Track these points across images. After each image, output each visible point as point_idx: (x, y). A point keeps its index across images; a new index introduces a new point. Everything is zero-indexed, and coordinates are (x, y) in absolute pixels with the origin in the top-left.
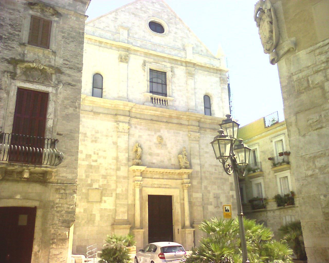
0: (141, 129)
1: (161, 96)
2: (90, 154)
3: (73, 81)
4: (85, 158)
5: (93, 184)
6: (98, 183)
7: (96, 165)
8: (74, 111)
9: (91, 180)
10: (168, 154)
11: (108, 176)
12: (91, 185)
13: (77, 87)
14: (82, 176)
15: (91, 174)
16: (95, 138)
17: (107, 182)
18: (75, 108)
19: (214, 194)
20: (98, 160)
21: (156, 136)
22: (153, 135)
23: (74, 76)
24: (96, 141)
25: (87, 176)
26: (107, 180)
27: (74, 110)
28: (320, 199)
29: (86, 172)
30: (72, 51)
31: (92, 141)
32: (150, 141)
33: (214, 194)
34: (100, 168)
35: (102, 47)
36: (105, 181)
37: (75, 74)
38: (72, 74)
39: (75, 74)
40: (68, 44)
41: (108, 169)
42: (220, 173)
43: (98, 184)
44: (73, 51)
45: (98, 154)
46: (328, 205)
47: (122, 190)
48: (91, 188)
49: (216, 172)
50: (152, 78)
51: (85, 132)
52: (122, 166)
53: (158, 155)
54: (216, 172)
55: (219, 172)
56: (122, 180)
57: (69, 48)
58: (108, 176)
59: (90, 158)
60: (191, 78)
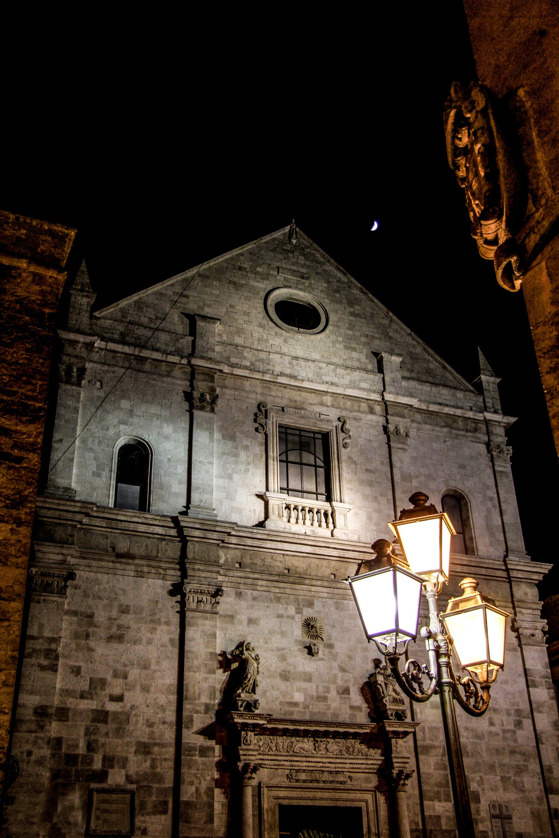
0: (254, 599)
1: (314, 502)
2: (101, 676)
3: (15, 446)
4: (87, 688)
5: (110, 770)
6: (124, 767)
7: (120, 710)
8: (12, 534)
9: (105, 759)
10: (340, 674)
11: (155, 744)
12: (102, 776)
13: (25, 465)
14: (77, 746)
15: (102, 740)
16: (119, 627)
17: (153, 767)
18: (14, 526)
19: (493, 806)
20: (126, 694)
21: (299, 620)
22: (293, 618)
23: (16, 432)
24: (120, 638)
25: (91, 747)
26: (153, 760)
27: (12, 530)
28: (35, 227)
29: (88, 732)
30: (16, 363)
31: (110, 639)
32: (283, 634)
33: (493, 806)
34: (133, 719)
35: (144, 372)
36: (146, 761)
37: (21, 428)
38: (14, 428)
39: (21, 428)
40: (9, 345)
41: (154, 723)
42: (508, 735)
43: (123, 772)
44: (20, 364)
45: (125, 677)
46: (556, 158)
47: (197, 790)
48: (104, 785)
49: (493, 729)
50: (286, 452)
51: (89, 611)
52: (197, 712)
53: (308, 678)
54: (493, 729)
55: (504, 731)
56: (197, 758)
57: (9, 358)
58: (155, 744)
59: (104, 690)
60: (400, 446)
